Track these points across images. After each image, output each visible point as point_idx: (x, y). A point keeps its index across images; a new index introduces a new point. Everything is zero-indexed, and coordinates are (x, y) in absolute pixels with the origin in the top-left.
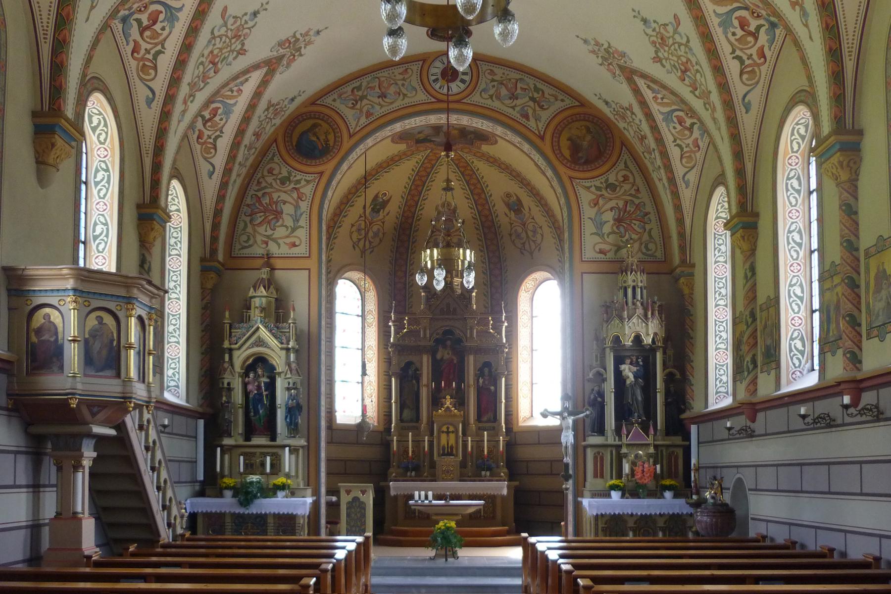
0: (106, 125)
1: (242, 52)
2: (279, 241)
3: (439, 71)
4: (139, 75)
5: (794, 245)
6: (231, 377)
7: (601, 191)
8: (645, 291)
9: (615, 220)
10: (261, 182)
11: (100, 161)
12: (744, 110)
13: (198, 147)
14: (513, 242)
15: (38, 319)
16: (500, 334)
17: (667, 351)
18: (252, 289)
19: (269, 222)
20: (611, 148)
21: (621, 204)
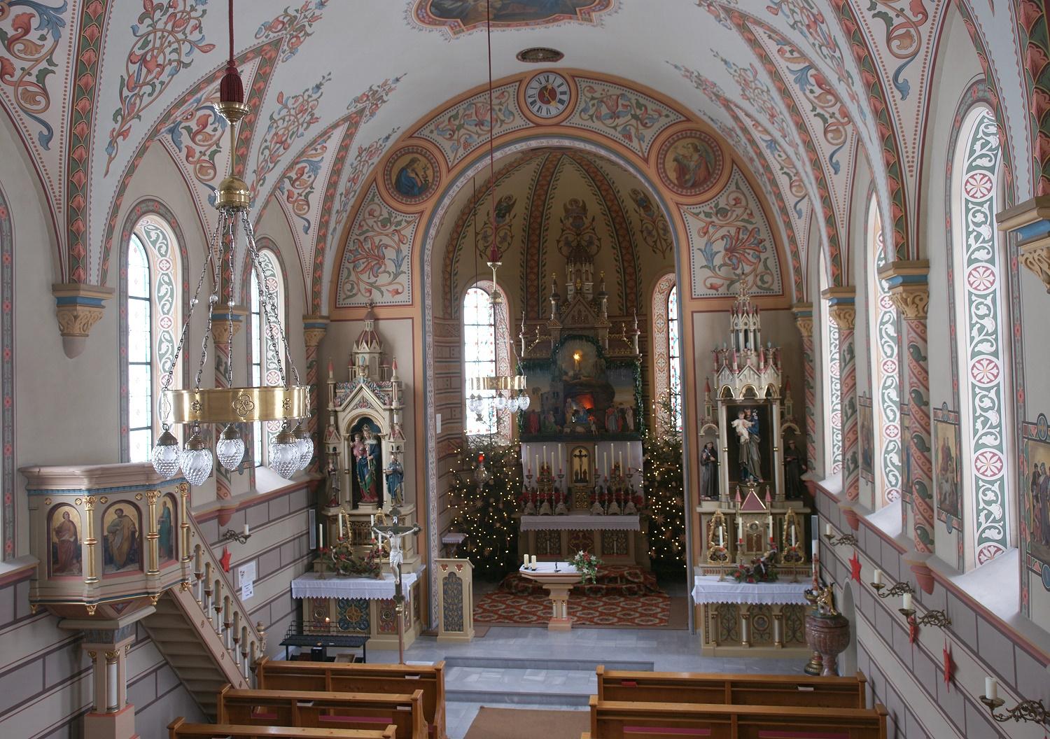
0: (165, 238)
1: (314, 120)
2: (383, 289)
3: (535, 92)
4: (198, 178)
5: (888, 339)
6: (337, 441)
7: (711, 217)
8: (759, 335)
9: (726, 250)
10: (362, 226)
11: (163, 274)
12: (832, 171)
13: (290, 206)
14: (645, 239)
15: (58, 519)
16: (632, 342)
17: (785, 402)
18: (355, 346)
19: (372, 269)
20: (721, 163)
21: (733, 231)
